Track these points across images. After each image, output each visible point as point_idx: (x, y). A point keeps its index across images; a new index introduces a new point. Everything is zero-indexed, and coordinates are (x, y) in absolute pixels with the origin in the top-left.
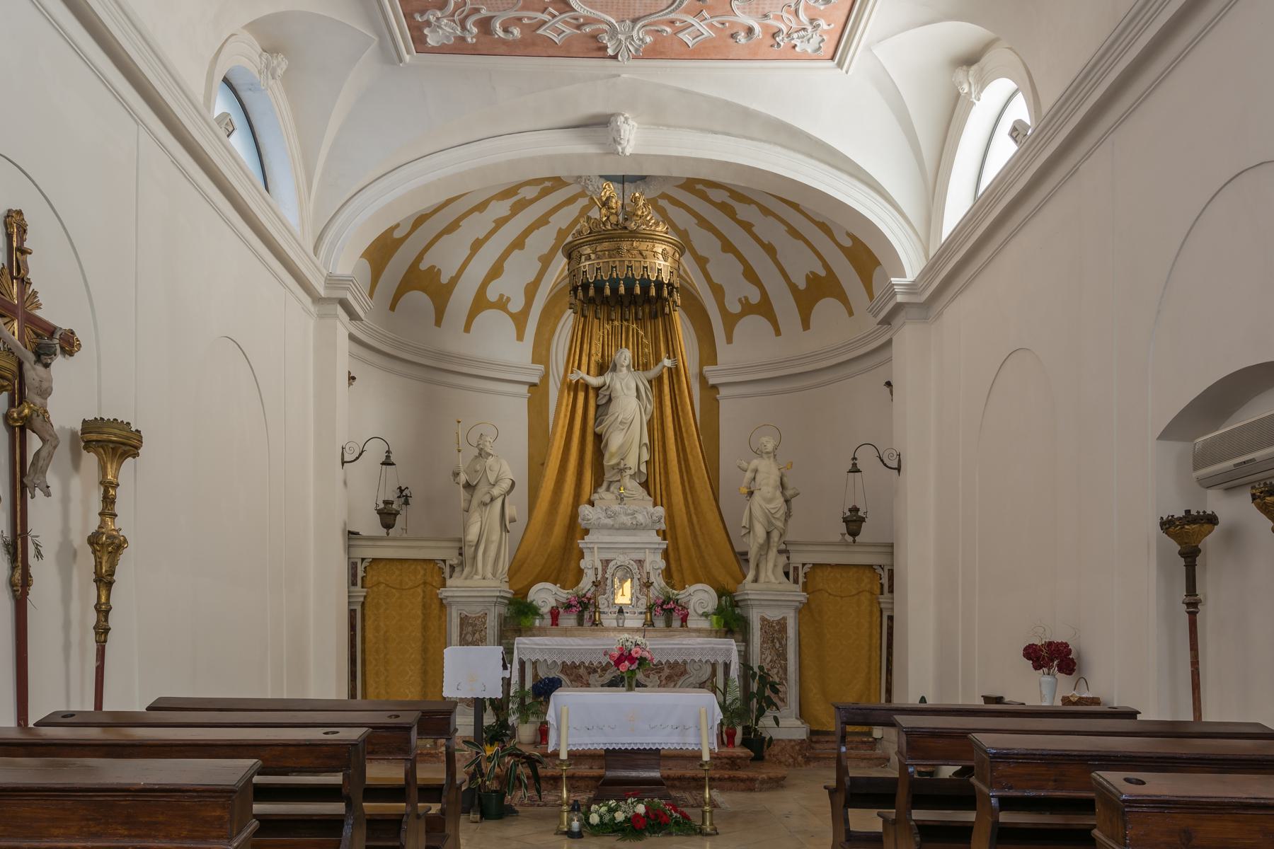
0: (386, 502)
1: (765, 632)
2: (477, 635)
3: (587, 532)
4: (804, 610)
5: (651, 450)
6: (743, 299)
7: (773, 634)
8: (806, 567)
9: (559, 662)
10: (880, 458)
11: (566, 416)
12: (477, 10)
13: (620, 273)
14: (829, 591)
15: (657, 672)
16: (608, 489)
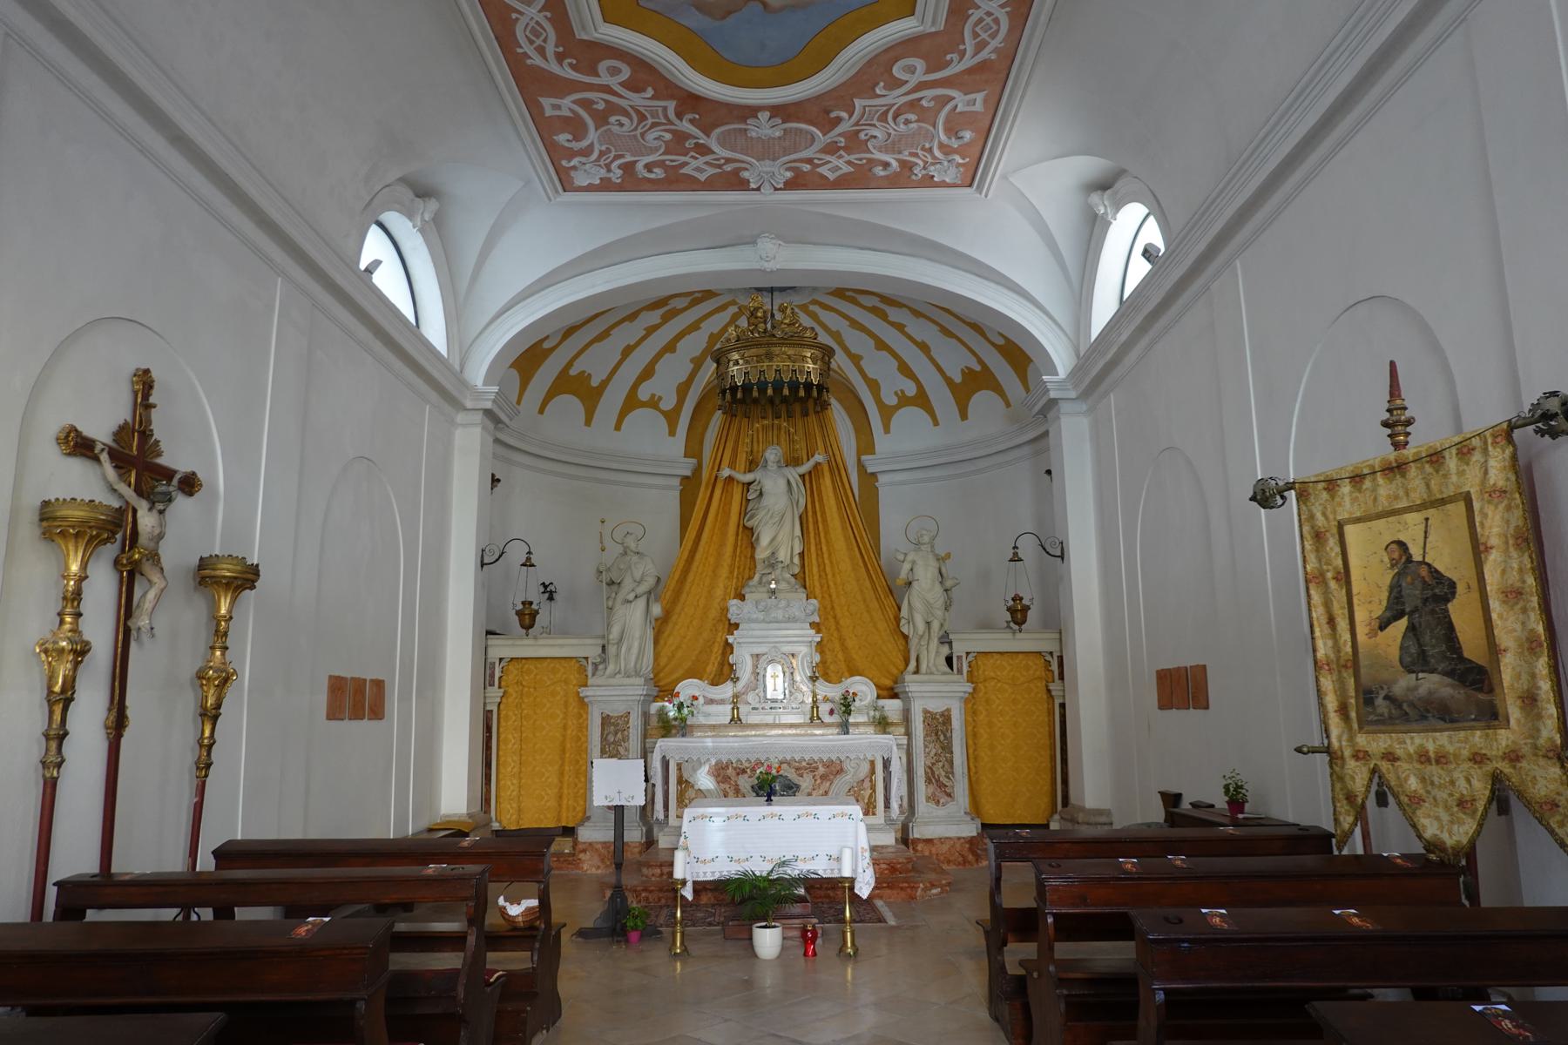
2: (619, 735)
4: (970, 701)
6: (899, 392)
8: (970, 655)
12: (622, 156)
15: (811, 771)
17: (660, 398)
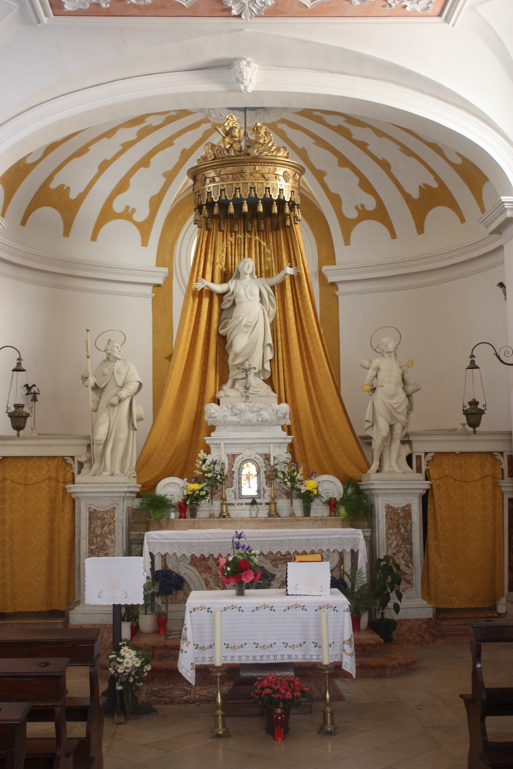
0: (17, 406)
1: (391, 518)
2: (106, 528)
3: (212, 428)
5: (275, 348)
6: (360, 207)
7: (398, 520)
8: (428, 456)
9: (189, 555)
10: (497, 355)
11: (191, 320)
13: (244, 194)
14: (455, 477)
16: (233, 386)
17: (134, 210)
